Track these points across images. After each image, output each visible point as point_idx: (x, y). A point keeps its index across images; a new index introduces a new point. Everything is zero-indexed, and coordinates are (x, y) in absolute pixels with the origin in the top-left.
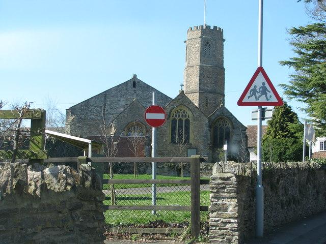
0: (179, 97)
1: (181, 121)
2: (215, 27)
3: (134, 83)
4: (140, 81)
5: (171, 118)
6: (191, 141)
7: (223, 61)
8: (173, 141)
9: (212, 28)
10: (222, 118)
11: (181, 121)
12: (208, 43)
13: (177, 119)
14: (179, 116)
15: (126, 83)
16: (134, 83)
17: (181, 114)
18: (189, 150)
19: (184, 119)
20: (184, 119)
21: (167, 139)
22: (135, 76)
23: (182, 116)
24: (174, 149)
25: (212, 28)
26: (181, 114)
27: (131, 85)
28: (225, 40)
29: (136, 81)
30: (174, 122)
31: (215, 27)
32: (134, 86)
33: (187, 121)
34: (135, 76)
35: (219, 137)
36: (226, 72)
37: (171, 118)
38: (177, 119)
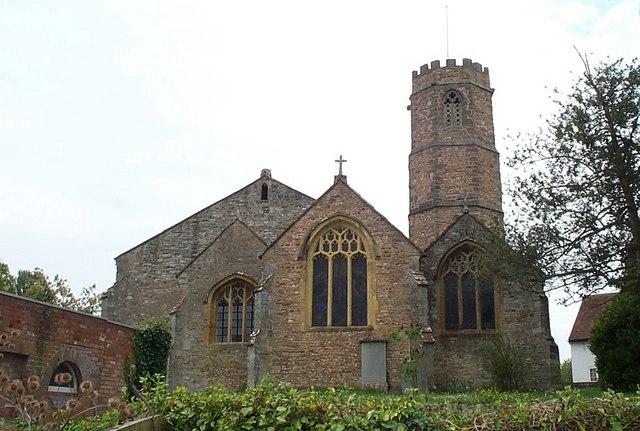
0: (335, 192)
1: (340, 260)
2: (467, 62)
3: (265, 188)
4: (277, 184)
5: (312, 254)
6: (371, 320)
7: (493, 136)
8: (318, 318)
9: (459, 63)
10: (466, 249)
11: (340, 260)
12: (452, 96)
13: (330, 255)
14: (335, 248)
15: (245, 191)
16: (265, 188)
17: (340, 242)
18: (364, 348)
19: (349, 255)
20: (349, 255)
21: (297, 316)
22: (266, 174)
23: (345, 248)
24: (322, 345)
25: (459, 63)
26: (340, 242)
27: (256, 195)
28: (493, 90)
29: (269, 183)
30: (320, 262)
31: (467, 62)
32: (264, 196)
33: (360, 261)
34: (266, 174)
35: (460, 304)
36: (496, 100)
37: (312, 254)
38: (330, 255)
